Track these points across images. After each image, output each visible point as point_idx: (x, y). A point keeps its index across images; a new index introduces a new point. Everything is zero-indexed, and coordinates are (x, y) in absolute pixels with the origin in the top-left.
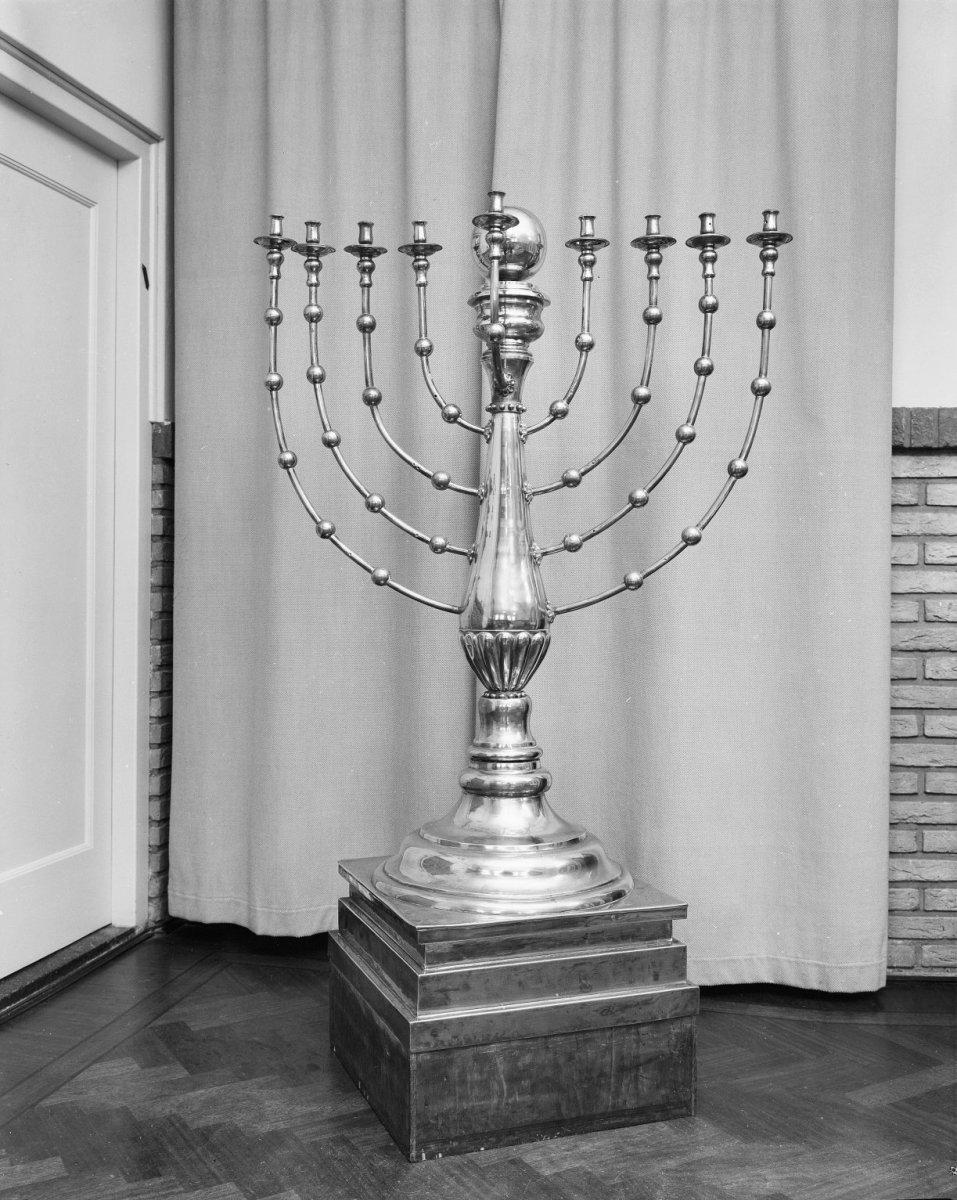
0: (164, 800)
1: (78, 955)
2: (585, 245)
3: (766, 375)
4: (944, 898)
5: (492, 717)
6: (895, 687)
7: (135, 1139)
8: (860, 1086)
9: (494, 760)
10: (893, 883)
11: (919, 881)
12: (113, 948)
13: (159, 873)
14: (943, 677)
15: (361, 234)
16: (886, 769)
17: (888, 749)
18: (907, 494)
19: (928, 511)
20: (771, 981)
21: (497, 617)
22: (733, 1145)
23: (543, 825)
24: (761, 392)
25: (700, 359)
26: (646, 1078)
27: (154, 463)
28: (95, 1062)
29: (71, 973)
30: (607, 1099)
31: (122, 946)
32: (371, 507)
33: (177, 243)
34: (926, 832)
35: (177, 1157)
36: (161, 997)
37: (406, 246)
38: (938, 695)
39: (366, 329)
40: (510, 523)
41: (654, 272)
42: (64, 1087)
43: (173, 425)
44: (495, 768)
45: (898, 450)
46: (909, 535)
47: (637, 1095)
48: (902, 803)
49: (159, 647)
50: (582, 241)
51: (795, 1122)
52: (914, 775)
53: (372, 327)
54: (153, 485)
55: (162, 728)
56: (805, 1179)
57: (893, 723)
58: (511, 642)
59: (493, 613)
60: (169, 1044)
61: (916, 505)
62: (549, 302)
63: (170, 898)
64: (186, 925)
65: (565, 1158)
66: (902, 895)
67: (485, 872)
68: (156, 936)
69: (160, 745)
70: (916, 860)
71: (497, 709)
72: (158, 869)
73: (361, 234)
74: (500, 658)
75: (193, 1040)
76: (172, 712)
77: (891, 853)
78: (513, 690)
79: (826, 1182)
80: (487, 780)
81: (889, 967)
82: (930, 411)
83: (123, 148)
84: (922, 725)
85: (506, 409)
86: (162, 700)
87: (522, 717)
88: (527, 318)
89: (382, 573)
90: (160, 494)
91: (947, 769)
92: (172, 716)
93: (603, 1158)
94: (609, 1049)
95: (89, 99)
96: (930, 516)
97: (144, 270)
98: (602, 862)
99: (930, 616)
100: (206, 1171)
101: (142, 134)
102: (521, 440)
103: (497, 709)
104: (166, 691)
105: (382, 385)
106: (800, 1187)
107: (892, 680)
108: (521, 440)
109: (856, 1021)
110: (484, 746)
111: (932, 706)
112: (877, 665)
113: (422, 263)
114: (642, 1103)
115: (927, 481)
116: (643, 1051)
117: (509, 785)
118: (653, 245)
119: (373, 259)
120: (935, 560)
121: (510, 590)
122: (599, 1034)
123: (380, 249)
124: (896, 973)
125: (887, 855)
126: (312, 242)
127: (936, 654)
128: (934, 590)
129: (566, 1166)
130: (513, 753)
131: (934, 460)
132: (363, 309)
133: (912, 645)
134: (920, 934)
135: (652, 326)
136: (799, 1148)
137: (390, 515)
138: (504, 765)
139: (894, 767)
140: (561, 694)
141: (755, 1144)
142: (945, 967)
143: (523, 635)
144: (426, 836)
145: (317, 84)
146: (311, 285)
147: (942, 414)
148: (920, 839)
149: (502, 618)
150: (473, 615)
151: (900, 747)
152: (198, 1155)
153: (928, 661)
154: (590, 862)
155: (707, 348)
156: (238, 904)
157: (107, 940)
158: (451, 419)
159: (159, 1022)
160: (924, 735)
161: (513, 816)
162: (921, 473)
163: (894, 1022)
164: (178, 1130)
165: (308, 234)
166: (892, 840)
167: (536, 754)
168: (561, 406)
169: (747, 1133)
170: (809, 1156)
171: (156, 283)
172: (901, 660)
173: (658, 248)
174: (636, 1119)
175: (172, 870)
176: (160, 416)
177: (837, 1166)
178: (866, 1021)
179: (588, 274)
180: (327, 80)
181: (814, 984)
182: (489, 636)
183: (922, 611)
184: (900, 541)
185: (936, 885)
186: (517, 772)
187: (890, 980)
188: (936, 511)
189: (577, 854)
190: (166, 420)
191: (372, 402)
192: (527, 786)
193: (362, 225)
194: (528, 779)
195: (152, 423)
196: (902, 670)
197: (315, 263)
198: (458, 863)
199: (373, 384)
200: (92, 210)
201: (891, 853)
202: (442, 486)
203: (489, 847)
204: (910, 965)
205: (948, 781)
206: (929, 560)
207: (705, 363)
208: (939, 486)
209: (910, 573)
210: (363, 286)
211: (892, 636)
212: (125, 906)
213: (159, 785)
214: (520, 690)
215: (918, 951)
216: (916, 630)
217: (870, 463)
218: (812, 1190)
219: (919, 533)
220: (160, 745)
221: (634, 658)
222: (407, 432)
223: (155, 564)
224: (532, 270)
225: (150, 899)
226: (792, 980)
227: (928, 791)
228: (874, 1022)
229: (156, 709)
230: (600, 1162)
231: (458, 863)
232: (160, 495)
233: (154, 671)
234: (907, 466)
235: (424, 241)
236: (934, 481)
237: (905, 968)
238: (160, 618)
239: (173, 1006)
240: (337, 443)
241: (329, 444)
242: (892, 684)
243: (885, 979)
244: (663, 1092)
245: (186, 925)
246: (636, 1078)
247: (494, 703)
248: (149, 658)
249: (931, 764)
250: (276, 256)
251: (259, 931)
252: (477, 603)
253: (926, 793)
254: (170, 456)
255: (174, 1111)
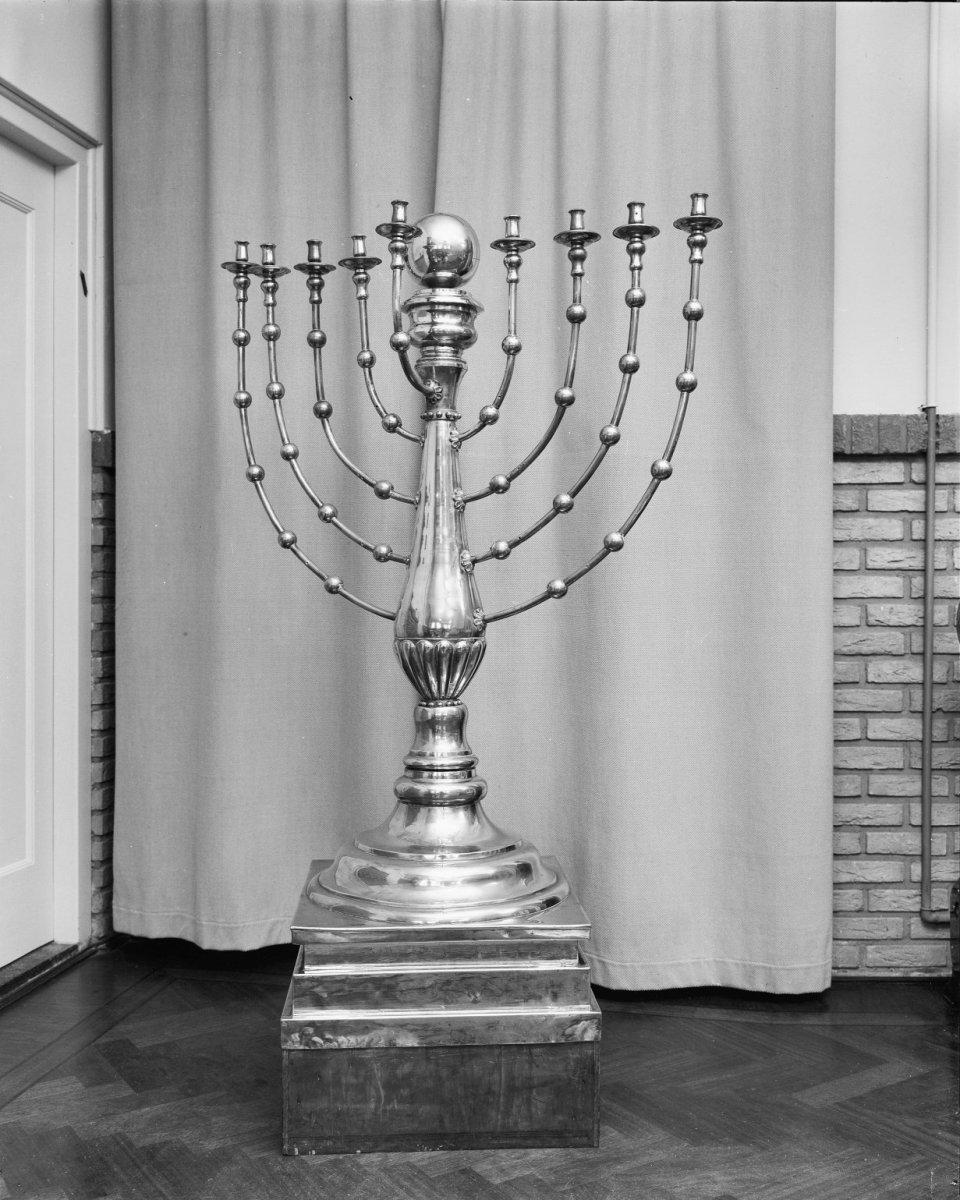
0: (107, 814)
1: (19, 973)
2: (507, 245)
3: (692, 370)
4: (888, 899)
5: (426, 727)
6: (838, 691)
7: (79, 1159)
8: (806, 1086)
9: (432, 769)
10: (837, 885)
11: (863, 883)
12: (56, 965)
13: (102, 889)
14: (885, 681)
15: (310, 252)
16: (829, 773)
17: (830, 753)
18: (849, 500)
19: (867, 517)
20: (718, 984)
21: (433, 626)
22: (682, 1149)
23: (477, 834)
24: (687, 388)
25: (626, 355)
26: (540, 1103)
27: (93, 472)
28: (38, 1081)
29: (13, 991)
30: (496, 1119)
31: (65, 963)
32: (325, 518)
33: (116, 249)
34: (869, 834)
35: (122, 1176)
36: (105, 1013)
37: (344, 261)
38: (880, 698)
39: (317, 344)
40: (444, 530)
41: (579, 269)
42: (6, 1108)
43: (113, 434)
44: (431, 777)
45: (839, 456)
46: (850, 541)
47: (530, 1117)
48: (848, 805)
49: (100, 659)
50: (506, 242)
51: (748, 1124)
52: (857, 778)
53: (322, 341)
54: (93, 495)
55: (104, 741)
56: (752, 1180)
57: (835, 726)
58: (450, 650)
59: (429, 619)
60: (114, 1062)
61: (857, 511)
62: (482, 310)
63: (115, 915)
64: (130, 941)
65: (514, 1167)
66: (846, 897)
67: (423, 883)
68: (98, 954)
69: (102, 759)
70: (860, 862)
71: (434, 717)
72: (101, 884)
73: (310, 252)
74: (434, 666)
75: (137, 1058)
76: (114, 724)
77: (835, 855)
78: (444, 699)
79: (773, 1182)
80: (422, 789)
81: (834, 968)
82: (870, 418)
83: (41, 142)
84: (865, 728)
85: (444, 417)
86: (103, 713)
87: (457, 726)
88: (461, 324)
89: (335, 582)
90: (100, 504)
91: (890, 772)
92: (114, 729)
93: (554, 1164)
94: (497, 1066)
95: (34, 110)
96: (871, 521)
97: (83, 276)
98: (537, 870)
99: (872, 620)
100: (153, 1189)
101: (77, 137)
102: (456, 447)
103: (434, 717)
104: (108, 704)
105: (332, 398)
106: (748, 1187)
107: (835, 684)
108: (456, 447)
109: (802, 1022)
110: (422, 755)
111: (875, 709)
112: (820, 671)
113: (363, 276)
114: (536, 1127)
115: (867, 487)
116: (537, 1073)
117: (442, 794)
118: (575, 241)
119: (323, 277)
120: (877, 565)
121: (446, 600)
122: (487, 1050)
123: (328, 266)
124: (841, 974)
125: (830, 857)
126: (267, 264)
127: (879, 657)
128: (875, 594)
129: (516, 1174)
130: (447, 761)
131: (874, 466)
132: (314, 326)
133: (855, 649)
134: (864, 935)
135: (576, 325)
136: (747, 1150)
137: (341, 525)
138: (440, 774)
139: (837, 770)
140: (509, 704)
141: (704, 1147)
142: (889, 968)
143: (462, 644)
144: (361, 846)
145: (258, 90)
146: (268, 305)
147: (882, 421)
148: (863, 840)
149: (439, 626)
150: (411, 628)
151: (844, 750)
152: (144, 1174)
153: (870, 665)
154: (525, 870)
155: (632, 344)
156: (183, 918)
157: (49, 957)
158: (391, 429)
159: (103, 1040)
160: (867, 739)
161: (446, 825)
162: (861, 480)
163: (840, 1022)
164: (124, 1149)
165: (264, 256)
166: (836, 841)
167: (472, 763)
168: (491, 411)
169: (697, 1137)
170: (757, 1156)
171: (94, 291)
172: (844, 664)
173: (582, 244)
174: (529, 1142)
175: (117, 886)
176: (100, 426)
177: (785, 1166)
178: (811, 1021)
179: (514, 276)
180: (269, 88)
181: (760, 986)
182: (428, 644)
183: (864, 615)
184: (842, 547)
185: (879, 886)
186: (451, 781)
187: (835, 981)
188: (877, 517)
189: (511, 861)
190: (107, 428)
191: (323, 415)
192: (462, 794)
193: (311, 243)
194: (464, 788)
195: (92, 432)
196: (845, 673)
197: (271, 284)
198: (394, 874)
199: (323, 397)
200: (29, 216)
201: (835, 855)
202: (383, 495)
203: (428, 857)
204: (855, 966)
205: (891, 783)
206: (871, 565)
207: (631, 359)
208: (880, 492)
209: (852, 578)
210: (313, 302)
211: (835, 640)
212: (65, 921)
213: (101, 800)
214: (455, 699)
215: (863, 952)
216: (860, 634)
217: (809, 475)
218: (760, 1190)
219: (860, 538)
220: (102, 759)
221: (583, 669)
222: (352, 439)
223: (95, 574)
224: (464, 277)
225: (93, 915)
226: (739, 982)
227: (871, 793)
228: (819, 1023)
229: (97, 722)
230: (551, 1169)
231: (394, 874)
232: (100, 505)
233: (96, 683)
234: (848, 472)
235: (364, 255)
236: (875, 487)
237: (850, 968)
238: (101, 629)
239: (117, 1023)
240: (295, 455)
241: (287, 457)
242: (835, 688)
243: (830, 980)
244: (560, 1118)
245: (130, 941)
246: (529, 1102)
247: (430, 712)
248: (90, 670)
249: (874, 767)
250: (242, 280)
251: (206, 945)
252: (411, 611)
253: (869, 795)
254: (110, 464)
255: (119, 1130)
